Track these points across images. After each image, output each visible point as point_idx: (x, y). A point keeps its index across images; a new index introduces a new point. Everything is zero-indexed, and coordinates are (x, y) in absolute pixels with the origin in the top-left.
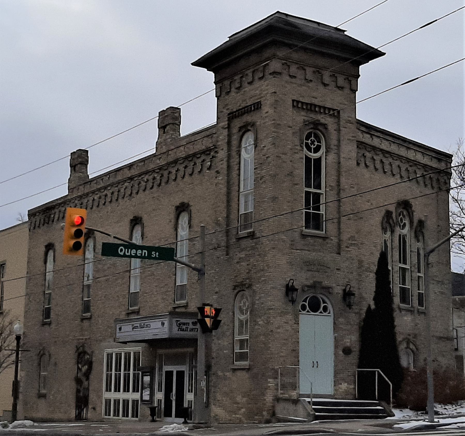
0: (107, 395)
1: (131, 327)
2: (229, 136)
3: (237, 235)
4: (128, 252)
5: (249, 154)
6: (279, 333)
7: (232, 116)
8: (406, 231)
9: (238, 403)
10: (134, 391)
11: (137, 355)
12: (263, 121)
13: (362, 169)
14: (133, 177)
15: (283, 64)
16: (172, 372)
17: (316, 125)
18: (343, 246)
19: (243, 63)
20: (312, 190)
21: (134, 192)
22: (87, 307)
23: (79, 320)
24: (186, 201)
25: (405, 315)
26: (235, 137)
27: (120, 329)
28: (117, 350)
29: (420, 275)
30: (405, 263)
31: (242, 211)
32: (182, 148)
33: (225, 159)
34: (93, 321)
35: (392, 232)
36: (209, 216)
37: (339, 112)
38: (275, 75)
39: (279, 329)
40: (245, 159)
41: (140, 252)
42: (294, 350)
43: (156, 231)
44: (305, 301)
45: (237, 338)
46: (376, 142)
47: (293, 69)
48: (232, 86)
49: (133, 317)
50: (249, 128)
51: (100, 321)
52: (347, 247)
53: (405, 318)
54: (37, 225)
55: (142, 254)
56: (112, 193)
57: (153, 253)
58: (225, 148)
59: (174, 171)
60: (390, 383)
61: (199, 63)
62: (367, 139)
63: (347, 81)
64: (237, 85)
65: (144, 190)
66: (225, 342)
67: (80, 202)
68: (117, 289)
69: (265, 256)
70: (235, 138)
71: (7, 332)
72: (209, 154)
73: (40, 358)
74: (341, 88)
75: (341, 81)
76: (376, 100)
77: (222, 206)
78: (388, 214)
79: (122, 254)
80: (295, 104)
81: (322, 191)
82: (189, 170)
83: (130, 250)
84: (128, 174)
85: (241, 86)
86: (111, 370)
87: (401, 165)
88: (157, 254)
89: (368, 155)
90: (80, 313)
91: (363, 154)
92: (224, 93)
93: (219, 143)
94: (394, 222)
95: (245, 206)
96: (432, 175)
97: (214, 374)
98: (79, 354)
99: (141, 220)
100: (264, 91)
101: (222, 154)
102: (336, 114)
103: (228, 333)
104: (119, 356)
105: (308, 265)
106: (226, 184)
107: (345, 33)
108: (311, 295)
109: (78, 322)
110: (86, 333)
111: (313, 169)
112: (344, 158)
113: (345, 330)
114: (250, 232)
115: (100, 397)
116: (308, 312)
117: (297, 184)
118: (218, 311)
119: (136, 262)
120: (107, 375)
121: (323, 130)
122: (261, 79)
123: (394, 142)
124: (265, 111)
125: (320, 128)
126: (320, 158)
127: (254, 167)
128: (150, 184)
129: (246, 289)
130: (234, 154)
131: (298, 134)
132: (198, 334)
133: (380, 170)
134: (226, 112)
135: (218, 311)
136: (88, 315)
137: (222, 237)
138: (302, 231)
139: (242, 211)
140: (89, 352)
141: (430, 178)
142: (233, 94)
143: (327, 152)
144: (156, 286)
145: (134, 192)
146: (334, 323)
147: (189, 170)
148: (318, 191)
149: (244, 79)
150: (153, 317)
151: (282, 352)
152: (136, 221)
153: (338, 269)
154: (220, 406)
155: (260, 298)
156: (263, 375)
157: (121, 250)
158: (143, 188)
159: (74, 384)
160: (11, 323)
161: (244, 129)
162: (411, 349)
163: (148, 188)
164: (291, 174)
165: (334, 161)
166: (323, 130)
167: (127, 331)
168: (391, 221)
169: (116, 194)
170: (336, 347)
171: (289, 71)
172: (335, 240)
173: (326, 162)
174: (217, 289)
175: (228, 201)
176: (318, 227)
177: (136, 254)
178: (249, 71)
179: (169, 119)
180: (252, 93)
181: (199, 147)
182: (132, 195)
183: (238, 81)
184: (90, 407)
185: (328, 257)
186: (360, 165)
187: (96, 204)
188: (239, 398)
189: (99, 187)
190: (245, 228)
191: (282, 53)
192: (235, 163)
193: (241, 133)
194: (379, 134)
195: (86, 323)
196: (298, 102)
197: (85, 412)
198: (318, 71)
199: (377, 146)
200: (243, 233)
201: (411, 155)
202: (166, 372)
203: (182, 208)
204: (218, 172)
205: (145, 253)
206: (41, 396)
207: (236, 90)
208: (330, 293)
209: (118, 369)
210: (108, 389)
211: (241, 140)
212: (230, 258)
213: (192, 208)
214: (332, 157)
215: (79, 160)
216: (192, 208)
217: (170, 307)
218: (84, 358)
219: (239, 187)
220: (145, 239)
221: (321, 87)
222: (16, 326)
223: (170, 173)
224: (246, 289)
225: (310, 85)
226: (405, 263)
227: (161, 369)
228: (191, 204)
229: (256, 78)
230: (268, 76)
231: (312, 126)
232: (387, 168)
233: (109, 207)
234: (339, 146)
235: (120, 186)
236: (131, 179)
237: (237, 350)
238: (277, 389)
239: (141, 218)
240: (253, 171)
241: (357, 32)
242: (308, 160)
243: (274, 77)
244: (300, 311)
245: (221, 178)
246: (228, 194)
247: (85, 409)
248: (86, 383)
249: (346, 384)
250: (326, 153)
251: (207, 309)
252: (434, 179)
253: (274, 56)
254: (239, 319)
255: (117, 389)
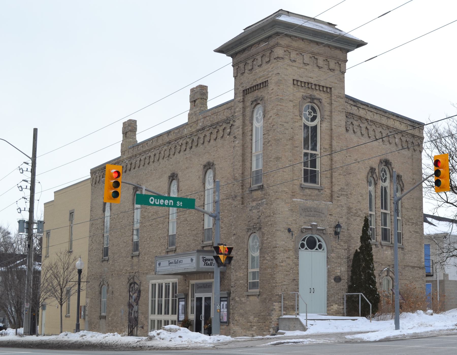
0: (152, 317)
1: (167, 263)
2: (244, 108)
3: (251, 187)
4: (157, 202)
5: (259, 123)
6: (282, 266)
7: (246, 92)
8: (387, 184)
9: (251, 322)
10: (172, 314)
11: (174, 285)
12: (269, 97)
13: (350, 134)
14: (171, 142)
15: (285, 51)
16: (201, 298)
17: (312, 99)
18: (335, 196)
19: (253, 50)
20: (310, 151)
21: (172, 153)
22: (136, 246)
23: (130, 257)
24: (211, 161)
25: (386, 250)
26: (248, 109)
27: (159, 264)
28: (160, 281)
29: (398, 218)
30: (386, 209)
31: (254, 169)
32: (208, 118)
33: (241, 127)
34: (140, 258)
35: (376, 184)
36: (229, 173)
37: (331, 88)
38: (278, 60)
39: (282, 262)
40: (256, 127)
41: (168, 202)
42: (294, 280)
43: (188, 184)
44: (304, 240)
45: (250, 270)
46: (362, 113)
47: (293, 55)
48: (246, 68)
49: (170, 254)
50: (259, 102)
51: (146, 258)
52: (338, 197)
53: (386, 252)
54: (97, 181)
55: (168, 204)
56: (155, 155)
57: (178, 202)
58: (241, 118)
59: (202, 136)
60: (370, 303)
61: (221, 50)
62: (354, 110)
63: (337, 64)
64: (250, 68)
65: (179, 152)
66: (241, 274)
67: (130, 162)
68: (159, 232)
69: (271, 204)
70: (248, 110)
71: (71, 268)
72: (229, 123)
73: (101, 288)
74: (332, 70)
75: (332, 64)
76: (362, 80)
77: (239, 165)
78: (372, 170)
79: (152, 203)
80: (328, 90)
81: (318, 152)
82: (214, 136)
83: (159, 200)
84: (167, 139)
85: (252, 69)
86: (155, 298)
87: (382, 131)
88: (181, 203)
89: (355, 123)
90: (131, 252)
91: (352, 123)
92: (239, 74)
93: (236, 114)
94: (377, 177)
95: (256, 165)
96: (408, 139)
97: (233, 299)
98: (131, 284)
99: (177, 177)
100: (270, 72)
101: (238, 123)
102: (328, 90)
103: (243, 267)
104: (160, 286)
105: (306, 210)
106: (241, 147)
107: (336, 27)
108: (309, 236)
109: (129, 259)
110: (135, 267)
111: (311, 136)
112: (335, 126)
113: (336, 263)
114: (260, 186)
115: (147, 318)
116: (306, 249)
117: (297, 147)
118: (230, 250)
119: (173, 210)
120: (152, 300)
121: (319, 104)
122: (268, 62)
123: (377, 113)
124: (271, 88)
125: (315, 101)
126: (316, 126)
127: (263, 134)
128: (184, 147)
129: (256, 232)
130: (247, 122)
131: (298, 106)
132: (214, 267)
133: (366, 135)
134: (241, 89)
135: (230, 250)
136: (137, 253)
137: (238, 189)
138: (301, 185)
139: (254, 169)
140: (138, 283)
141: (406, 141)
142: (246, 74)
143: (322, 121)
144: (188, 230)
145: (172, 153)
146: (328, 258)
147: (214, 136)
148: (313, 152)
149: (255, 63)
150: (185, 254)
151: (285, 281)
152: (173, 177)
153: (330, 215)
154: (237, 325)
155: (267, 238)
156: (270, 299)
157: (152, 200)
158: (178, 150)
159: (127, 308)
160: (75, 260)
161: (256, 102)
162: (391, 277)
163: (182, 150)
164: (292, 139)
165: (327, 128)
166: (319, 104)
167: (165, 266)
168: (374, 176)
169: (157, 155)
170: (329, 276)
171: (290, 57)
172: (328, 192)
173: (321, 129)
174: (234, 232)
175: (243, 161)
176: (313, 180)
177: (164, 203)
178: (258, 56)
179: (199, 95)
180: (261, 74)
181: (222, 117)
182: (170, 156)
183: (251, 64)
184: (139, 326)
185: (324, 204)
186: (349, 131)
187: (142, 163)
188: (251, 318)
189: (144, 150)
190: (256, 183)
191: (285, 41)
192: (249, 130)
193: (253, 106)
194: (364, 107)
195: (135, 259)
196: (298, 81)
197: (135, 331)
198: (314, 56)
199: (363, 116)
200: (255, 186)
201: (390, 123)
202: (197, 298)
203: (209, 166)
204: (235, 137)
205: (171, 202)
206: (101, 317)
207: (249, 72)
208: (324, 234)
209: (160, 296)
210: (153, 312)
211: (253, 111)
212: (245, 206)
213: (216, 166)
214: (325, 125)
215: (130, 128)
216: (216, 166)
217: (199, 246)
218: (134, 287)
219: (252, 150)
220: (180, 192)
221: (316, 69)
222: (78, 262)
223: (199, 138)
224: (256, 232)
225: (307, 67)
226: (386, 209)
227: (193, 296)
228: (215, 163)
229: (264, 62)
230: (273, 60)
231: (309, 100)
232: (371, 133)
233: (152, 166)
234: (331, 116)
235: (160, 149)
236: (169, 143)
237: (250, 281)
238: (281, 311)
239: (177, 175)
240: (262, 136)
241: (347, 27)
242: (306, 127)
243: (278, 61)
244: (300, 249)
245: (238, 142)
246: (243, 155)
247: (135, 328)
248: (135, 308)
249: (337, 305)
250: (321, 121)
251: (221, 247)
252: (410, 143)
253: (277, 45)
254: (252, 255)
255: (160, 312)
